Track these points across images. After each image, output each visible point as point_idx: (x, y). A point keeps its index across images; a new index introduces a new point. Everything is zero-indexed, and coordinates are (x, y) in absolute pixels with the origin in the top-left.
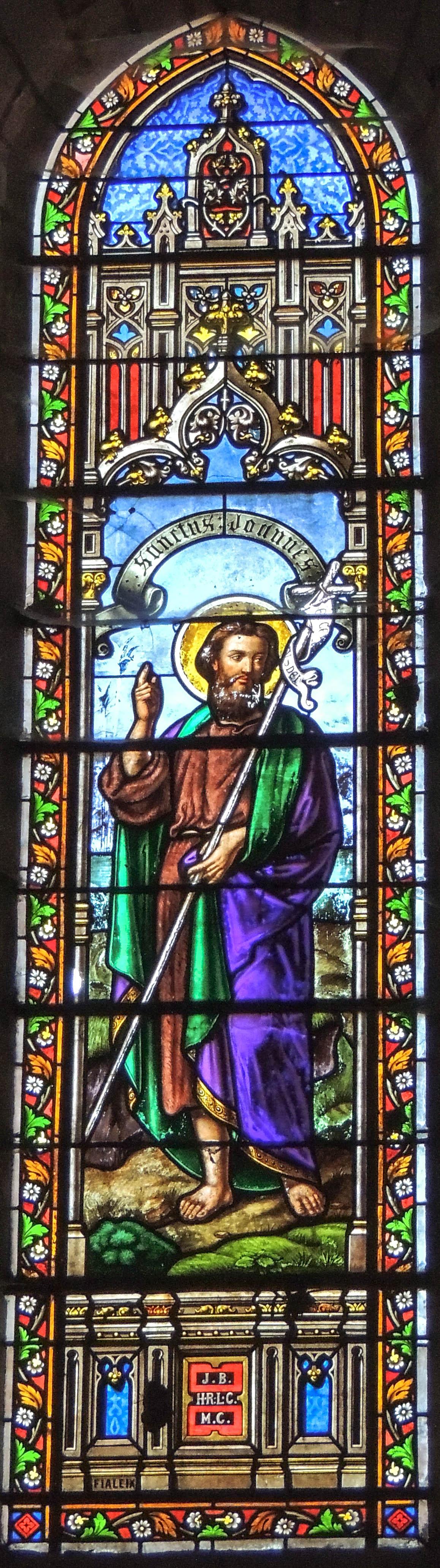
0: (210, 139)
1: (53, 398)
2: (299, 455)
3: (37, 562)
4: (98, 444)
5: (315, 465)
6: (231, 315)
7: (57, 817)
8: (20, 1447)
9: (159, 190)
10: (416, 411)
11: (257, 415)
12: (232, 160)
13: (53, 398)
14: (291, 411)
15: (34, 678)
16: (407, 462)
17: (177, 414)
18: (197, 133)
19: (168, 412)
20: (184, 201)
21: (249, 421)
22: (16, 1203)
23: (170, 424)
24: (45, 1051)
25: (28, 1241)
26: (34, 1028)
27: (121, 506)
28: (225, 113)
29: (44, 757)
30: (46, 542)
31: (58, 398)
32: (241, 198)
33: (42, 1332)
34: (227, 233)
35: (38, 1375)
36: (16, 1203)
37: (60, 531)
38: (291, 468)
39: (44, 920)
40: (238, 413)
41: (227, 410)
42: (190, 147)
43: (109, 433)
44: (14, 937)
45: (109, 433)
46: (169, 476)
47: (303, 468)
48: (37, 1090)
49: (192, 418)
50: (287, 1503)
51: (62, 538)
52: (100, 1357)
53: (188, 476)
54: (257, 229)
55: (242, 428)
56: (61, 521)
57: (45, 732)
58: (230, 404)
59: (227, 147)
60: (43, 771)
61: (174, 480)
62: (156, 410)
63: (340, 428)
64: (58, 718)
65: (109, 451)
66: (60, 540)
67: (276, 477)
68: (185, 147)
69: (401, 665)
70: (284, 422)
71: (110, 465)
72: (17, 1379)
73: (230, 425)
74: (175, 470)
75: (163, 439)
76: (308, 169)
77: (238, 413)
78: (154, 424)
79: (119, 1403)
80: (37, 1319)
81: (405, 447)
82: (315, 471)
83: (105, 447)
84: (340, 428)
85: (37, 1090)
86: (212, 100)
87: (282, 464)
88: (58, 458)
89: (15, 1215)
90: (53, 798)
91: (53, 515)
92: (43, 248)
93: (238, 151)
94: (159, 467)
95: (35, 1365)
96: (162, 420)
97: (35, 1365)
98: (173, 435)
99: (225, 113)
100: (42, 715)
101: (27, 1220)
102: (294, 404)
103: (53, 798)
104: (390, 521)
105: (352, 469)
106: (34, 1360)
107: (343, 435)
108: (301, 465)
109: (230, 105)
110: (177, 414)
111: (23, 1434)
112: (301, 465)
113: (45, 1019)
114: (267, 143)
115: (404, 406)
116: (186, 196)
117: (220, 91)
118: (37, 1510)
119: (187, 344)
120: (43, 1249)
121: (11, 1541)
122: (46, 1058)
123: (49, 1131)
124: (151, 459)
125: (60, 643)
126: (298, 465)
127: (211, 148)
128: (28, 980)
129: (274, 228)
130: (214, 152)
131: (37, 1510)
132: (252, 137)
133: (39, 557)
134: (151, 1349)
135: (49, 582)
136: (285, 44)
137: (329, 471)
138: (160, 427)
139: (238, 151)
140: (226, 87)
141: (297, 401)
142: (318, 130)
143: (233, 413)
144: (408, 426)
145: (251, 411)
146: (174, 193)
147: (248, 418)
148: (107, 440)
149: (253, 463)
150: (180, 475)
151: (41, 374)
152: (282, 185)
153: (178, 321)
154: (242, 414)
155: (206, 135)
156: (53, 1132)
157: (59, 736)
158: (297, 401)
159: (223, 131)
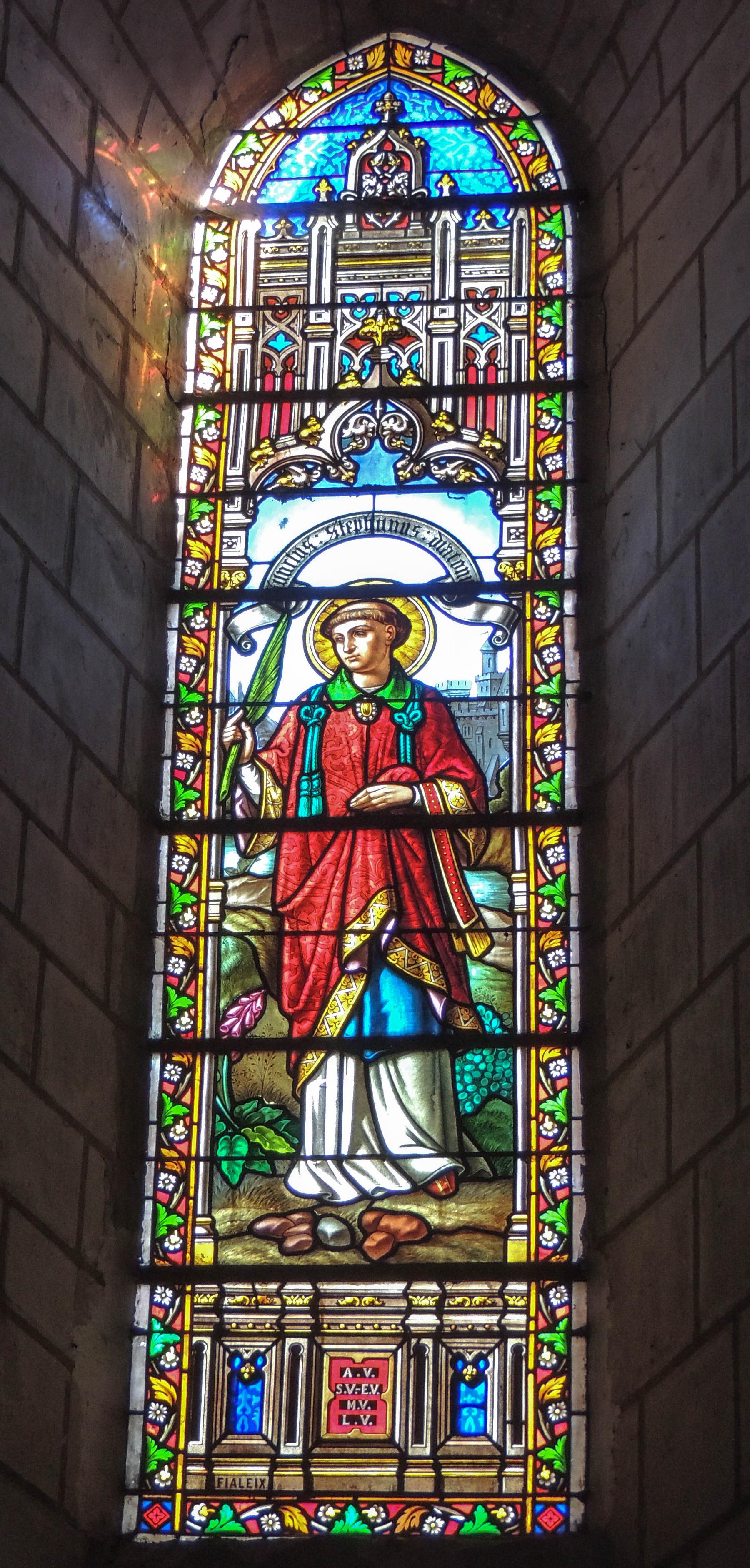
0: (370, 139)
1: (170, 1212)
2: (451, 460)
3: (190, 466)
4: (248, 452)
5: (467, 469)
6: (386, 328)
7: (192, 1012)
8: (172, 993)
9: (317, 185)
10: (570, 418)
11: (411, 423)
12: (391, 158)
13: (170, 1212)
14: (445, 418)
15: (166, 973)
16: (562, 857)
17: (328, 425)
18: (357, 135)
19: (321, 421)
20: (343, 194)
21: (402, 429)
22: (149, 1192)
23: (323, 432)
24: (169, 1374)
25: (163, 1231)
26: (189, 613)
27: (269, 506)
28: (387, 116)
29: (177, 1058)
30: (185, 732)
31: (190, 787)
32: (399, 191)
33: (171, 1443)
34: (383, 224)
35: (180, 1142)
36: (149, 1192)
37: (198, 721)
38: (443, 472)
39: (181, 1011)
40: (392, 420)
41: (381, 417)
42: (350, 147)
43: (259, 441)
44: (142, 1199)
45: (259, 441)
46: (319, 480)
47: (454, 472)
48: (183, 868)
49: (346, 425)
50: (414, 1356)
51: (201, 728)
52: (232, 1350)
53: (338, 480)
54: (415, 221)
55: (393, 434)
56: (210, 520)
57: (178, 1032)
58: (384, 412)
59: (388, 147)
60: (173, 1073)
61: (324, 484)
62: (308, 419)
63: (493, 433)
64: (180, 1235)
65: (260, 457)
66: (208, 539)
67: (427, 480)
68: (346, 147)
69: (548, 661)
70: (437, 428)
71: (260, 471)
72: (176, 728)
73: (383, 430)
74: (325, 474)
75: (316, 447)
76: (467, 165)
77: (392, 420)
78: (305, 433)
79: (249, 1401)
80: (189, 877)
81: (560, 840)
82: (468, 474)
83: (256, 454)
84: (493, 433)
85: (183, 868)
86: (374, 107)
87: (434, 469)
88: (194, 749)
89: (149, 1205)
90: (183, 1100)
91: (202, 515)
92: (152, 1257)
93: (397, 149)
94: (309, 472)
95: (178, 1132)
96: (314, 429)
97: (178, 1132)
98: (325, 443)
99: (387, 116)
100: (163, 1231)
101: (162, 1210)
102: (447, 413)
103: (183, 1100)
104: (543, 915)
105: (506, 472)
106: (177, 1127)
107: (495, 438)
108: (453, 469)
109: (391, 111)
110: (328, 425)
111: (175, 981)
112: (453, 469)
113: (200, 606)
114: (427, 143)
115: (560, 1005)
116: (345, 189)
117: (382, 99)
118: (167, 1500)
119: (342, 353)
120: (183, 1129)
121: (138, 1530)
122: (200, 640)
123: (188, 1120)
124: (302, 465)
125: (205, 640)
126: (450, 470)
127: (371, 148)
128: (162, 1074)
129: (432, 220)
130: (375, 151)
131: (167, 1500)
132: (411, 139)
133: (169, 952)
134: (290, 1341)
135: (166, 1309)
136: (448, 65)
137: (483, 474)
138: (312, 436)
139: (397, 149)
140: (387, 95)
141: (449, 410)
142: (479, 133)
143: (387, 420)
144: (563, 431)
145: (405, 419)
146: (332, 187)
147: (401, 425)
148: (257, 447)
149: (404, 468)
150: (330, 480)
151: (152, 1298)
152: (440, 180)
153: (334, 333)
154: (395, 421)
155: (366, 136)
156: (191, 1119)
157: (191, 1035)
158: (449, 410)
159: (383, 133)
